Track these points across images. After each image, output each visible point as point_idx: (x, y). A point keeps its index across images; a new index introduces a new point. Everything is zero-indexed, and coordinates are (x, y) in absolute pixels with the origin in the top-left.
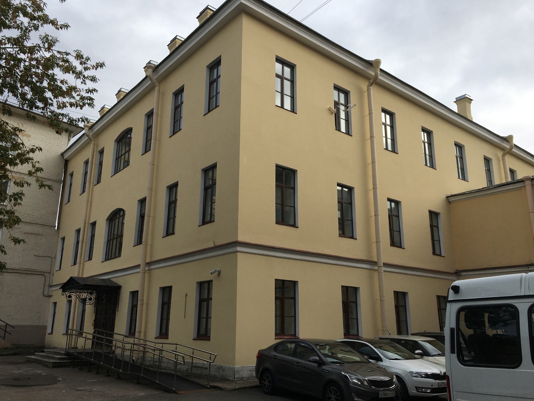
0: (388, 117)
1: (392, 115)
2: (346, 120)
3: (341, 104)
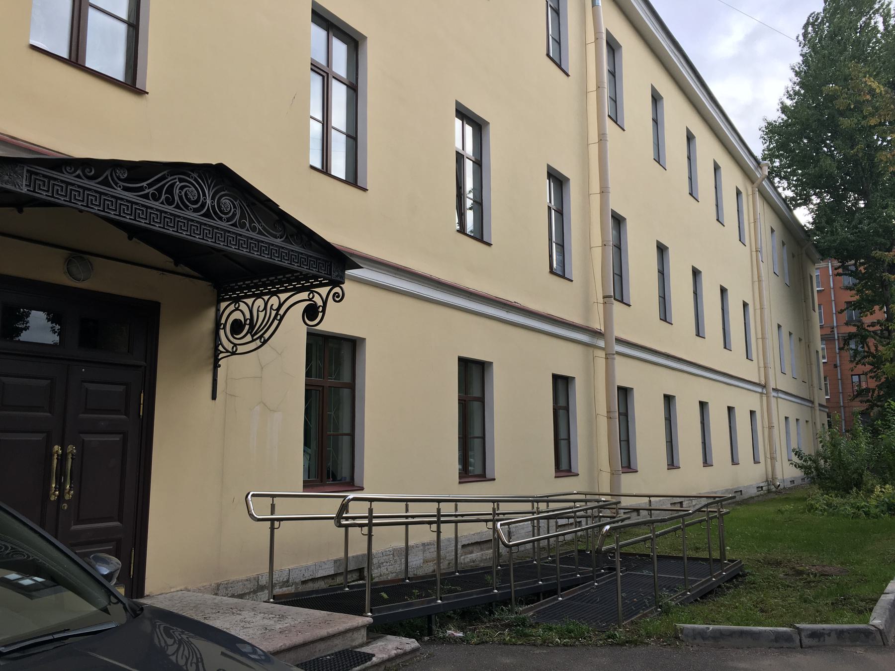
0: (469, 130)
1: (479, 126)
2: (348, 136)
3: (334, 77)
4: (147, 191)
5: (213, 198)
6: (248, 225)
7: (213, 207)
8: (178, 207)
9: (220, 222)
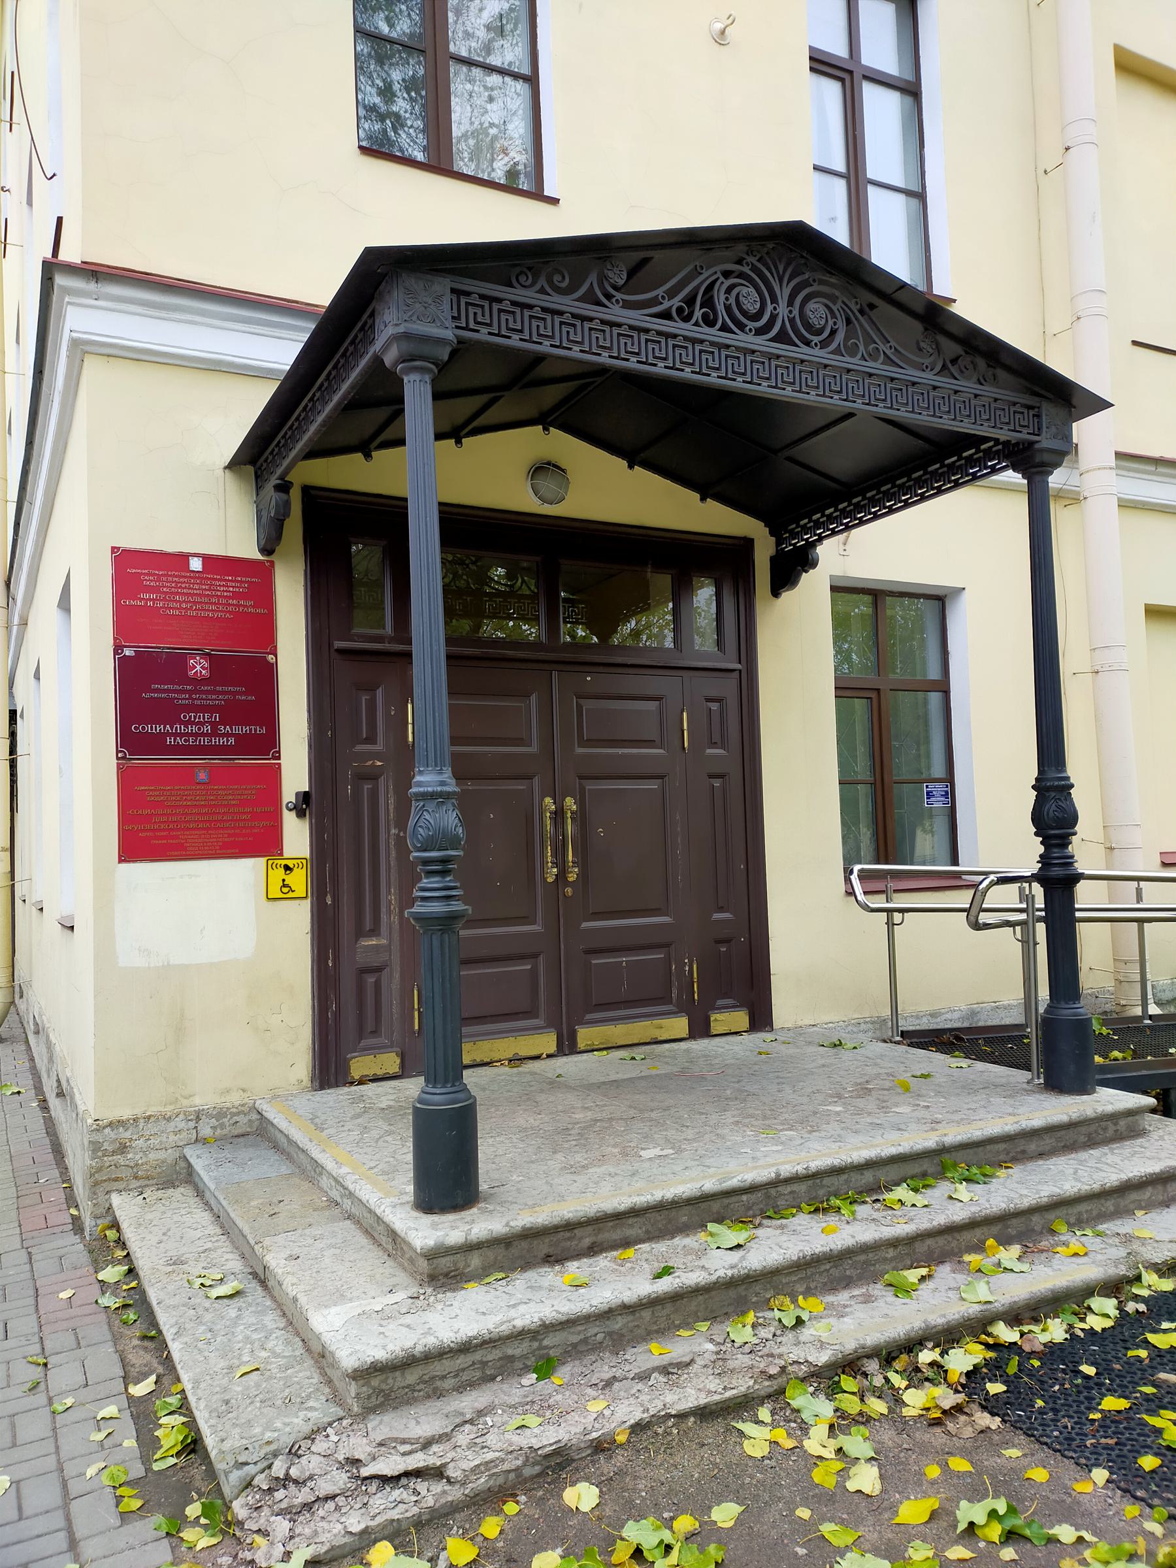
4: (666, 304)
5: (790, 303)
6: (862, 348)
7: (792, 321)
8: (724, 328)
9: (805, 349)
